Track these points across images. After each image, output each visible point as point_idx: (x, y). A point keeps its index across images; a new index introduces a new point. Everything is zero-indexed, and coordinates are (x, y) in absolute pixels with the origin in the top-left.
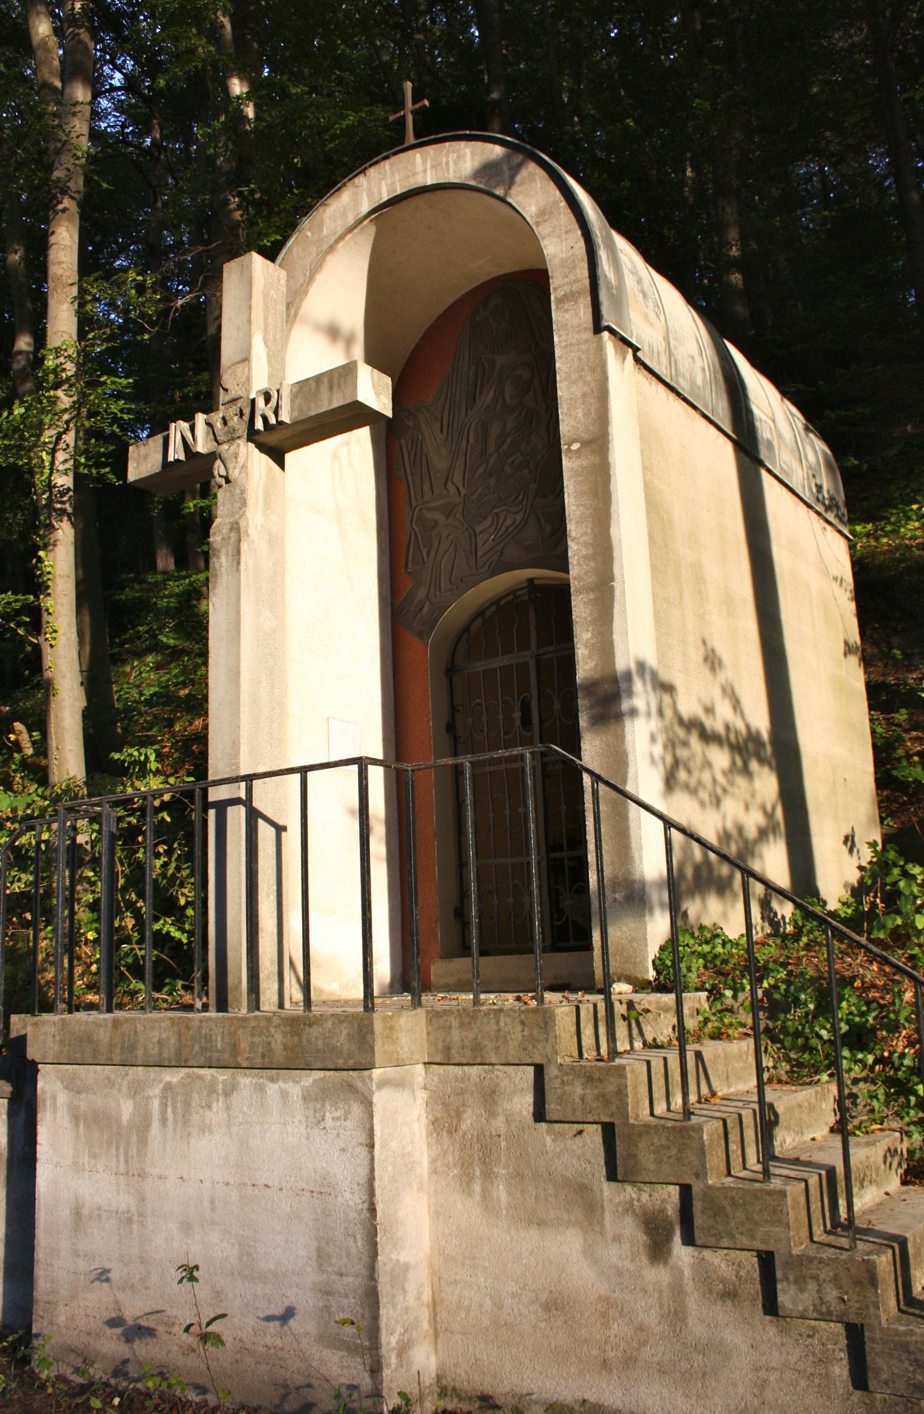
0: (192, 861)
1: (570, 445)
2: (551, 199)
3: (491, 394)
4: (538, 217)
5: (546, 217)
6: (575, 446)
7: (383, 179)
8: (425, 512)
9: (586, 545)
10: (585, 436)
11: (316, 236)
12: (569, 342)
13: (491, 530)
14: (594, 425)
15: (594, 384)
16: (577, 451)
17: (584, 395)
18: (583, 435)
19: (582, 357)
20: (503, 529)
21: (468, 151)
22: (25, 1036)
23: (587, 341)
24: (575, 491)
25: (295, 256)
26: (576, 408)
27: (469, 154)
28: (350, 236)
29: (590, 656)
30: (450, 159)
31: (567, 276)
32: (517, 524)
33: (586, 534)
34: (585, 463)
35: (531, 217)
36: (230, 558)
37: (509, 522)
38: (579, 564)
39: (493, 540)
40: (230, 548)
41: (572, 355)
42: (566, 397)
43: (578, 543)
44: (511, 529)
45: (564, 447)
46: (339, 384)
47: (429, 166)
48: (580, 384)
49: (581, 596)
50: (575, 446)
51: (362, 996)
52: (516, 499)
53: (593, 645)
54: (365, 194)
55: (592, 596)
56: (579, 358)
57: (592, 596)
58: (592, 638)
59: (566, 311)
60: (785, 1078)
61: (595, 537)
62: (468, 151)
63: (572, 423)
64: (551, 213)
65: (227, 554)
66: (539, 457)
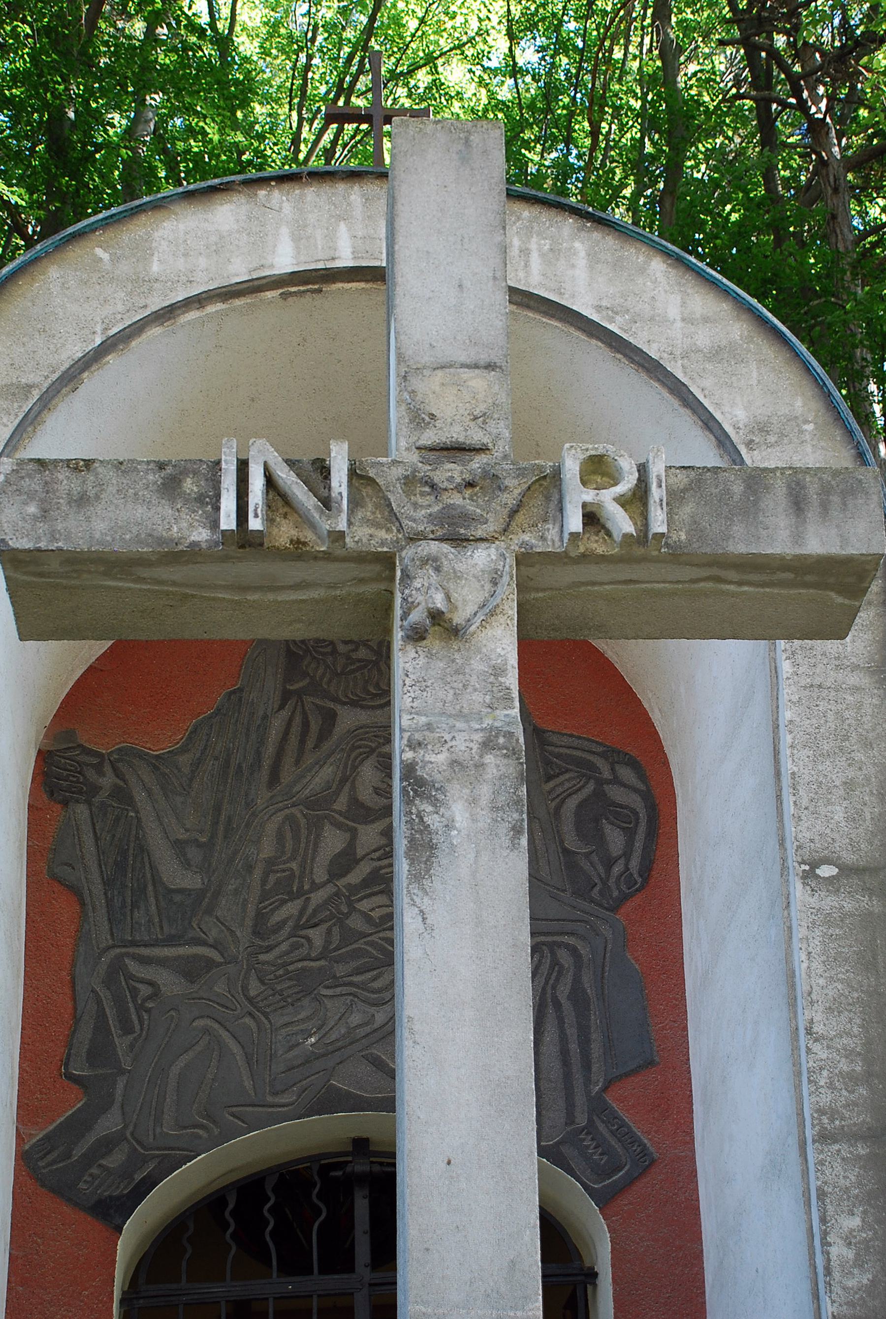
1: (814, 865)
2: (784, 410)
3: (327, 772)
5: (772, 439)
6: (826, 871)
7: (340, 218)
9: (849, 1054)
10: (849, 858)
11: (125, 268)
12: (817, 681)
15: (870, 770)
16: (830, 880)
17: (849, 785)
18: (844, 854)
19: (846, 714)
23: (855, 689)
24: (824, 952)
25: (55, 289)
26: (829, 803)
27: (583, 254)
28: (220, 306)
29: (859, 1263)
33: (848, 1034)
34: (848, 906)
35: (737, 428)
36: (485, 817)
37: (355, 1019)
38: (831, 1086)
40: (485, 791)
41: (823, 706)
42: (807, 778)
43: (828, 1047)
44: (361, 1032)
46: (825, 507)
48: (841, 762)
49: (836, 1147)
50: (826, 871)
52: (374, 979)
54: (285, 231)
55: (862, 1150)
58: (862, 1229)
61: (868, 1043)
63: (819, 827)
64: (782, 435)
65: (473, 801)
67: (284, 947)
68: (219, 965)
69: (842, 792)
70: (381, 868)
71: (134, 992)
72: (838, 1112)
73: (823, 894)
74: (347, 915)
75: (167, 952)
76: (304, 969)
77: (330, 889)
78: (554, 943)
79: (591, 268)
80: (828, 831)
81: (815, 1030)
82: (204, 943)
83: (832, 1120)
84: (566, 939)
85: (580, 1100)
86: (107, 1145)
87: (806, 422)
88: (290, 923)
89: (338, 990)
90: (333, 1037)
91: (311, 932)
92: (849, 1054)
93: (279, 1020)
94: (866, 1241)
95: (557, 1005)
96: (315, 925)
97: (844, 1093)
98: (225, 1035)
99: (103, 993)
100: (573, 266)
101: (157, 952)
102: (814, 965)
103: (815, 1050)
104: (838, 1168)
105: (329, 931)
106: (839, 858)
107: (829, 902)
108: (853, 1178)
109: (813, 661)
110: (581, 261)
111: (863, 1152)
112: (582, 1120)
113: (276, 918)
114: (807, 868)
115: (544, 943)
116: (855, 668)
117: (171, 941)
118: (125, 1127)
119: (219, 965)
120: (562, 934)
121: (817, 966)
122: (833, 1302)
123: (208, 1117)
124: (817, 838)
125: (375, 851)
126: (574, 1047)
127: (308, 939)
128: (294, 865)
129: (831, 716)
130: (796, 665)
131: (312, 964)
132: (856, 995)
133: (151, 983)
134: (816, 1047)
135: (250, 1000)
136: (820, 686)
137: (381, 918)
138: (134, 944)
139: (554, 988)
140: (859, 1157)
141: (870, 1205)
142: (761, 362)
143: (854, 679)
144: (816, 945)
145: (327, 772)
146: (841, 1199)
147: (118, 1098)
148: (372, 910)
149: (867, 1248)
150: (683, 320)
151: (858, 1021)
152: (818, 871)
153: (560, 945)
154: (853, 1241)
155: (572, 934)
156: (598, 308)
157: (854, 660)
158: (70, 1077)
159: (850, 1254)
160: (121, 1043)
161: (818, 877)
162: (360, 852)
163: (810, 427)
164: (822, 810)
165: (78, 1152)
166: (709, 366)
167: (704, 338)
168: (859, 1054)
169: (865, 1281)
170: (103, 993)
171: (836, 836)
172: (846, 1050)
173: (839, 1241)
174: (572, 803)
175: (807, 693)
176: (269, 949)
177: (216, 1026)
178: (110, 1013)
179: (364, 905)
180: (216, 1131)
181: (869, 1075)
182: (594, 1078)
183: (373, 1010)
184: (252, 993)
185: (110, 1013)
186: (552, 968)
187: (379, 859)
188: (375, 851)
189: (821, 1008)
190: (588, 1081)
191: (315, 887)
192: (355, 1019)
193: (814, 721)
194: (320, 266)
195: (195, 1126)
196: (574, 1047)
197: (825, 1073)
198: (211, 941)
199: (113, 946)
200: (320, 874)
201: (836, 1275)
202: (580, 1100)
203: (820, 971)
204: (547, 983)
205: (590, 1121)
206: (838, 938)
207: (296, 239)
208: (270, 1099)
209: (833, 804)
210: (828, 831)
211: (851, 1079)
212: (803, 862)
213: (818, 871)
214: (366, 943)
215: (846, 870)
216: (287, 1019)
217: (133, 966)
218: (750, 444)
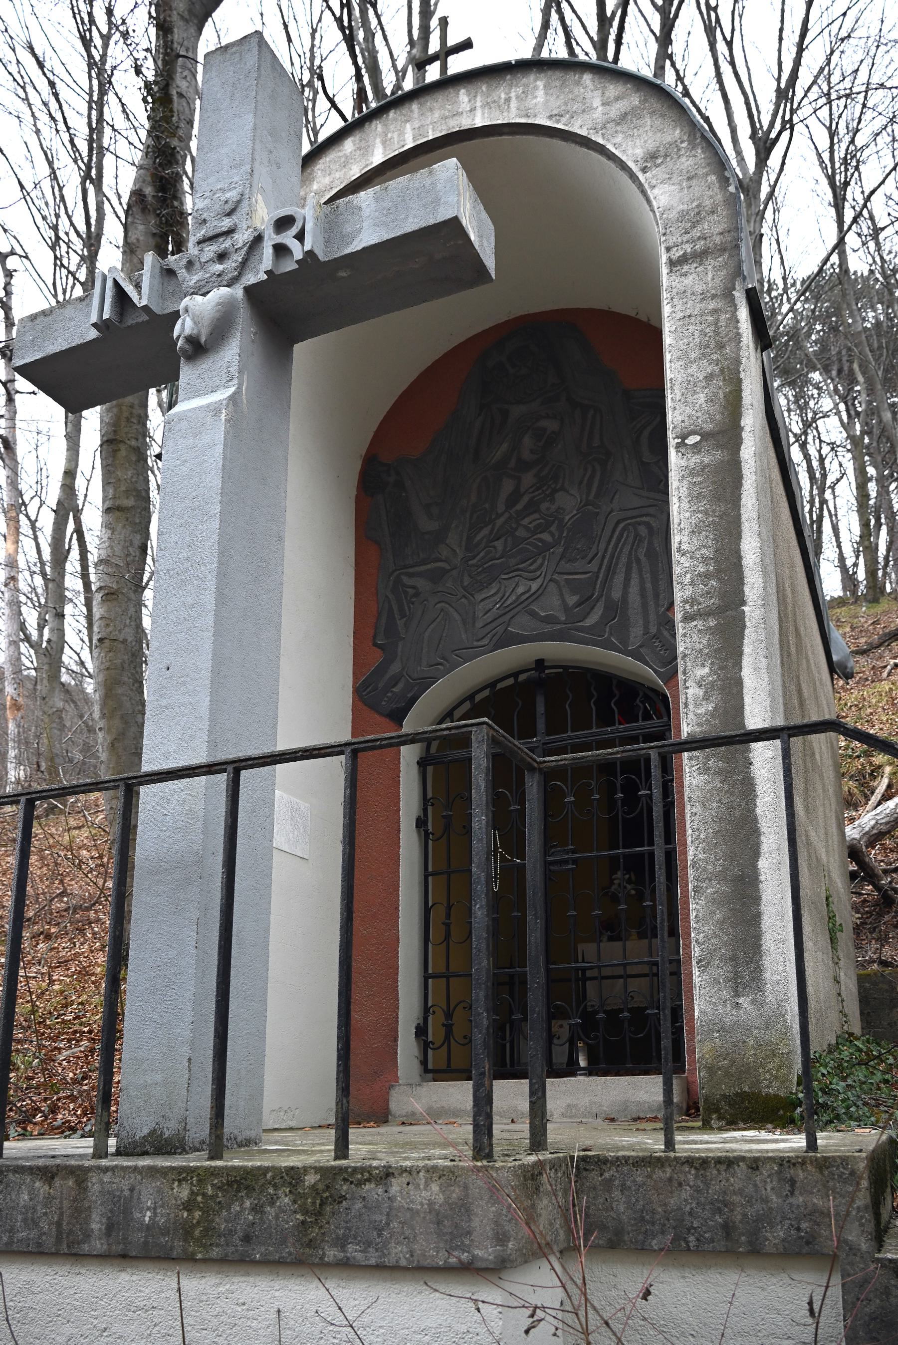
0: (855, 293)
1: (684, 437)
3: (505, 447)
4: (646, 161)
5: (659, 161)
6: (692, 440)
8: (405, 579)
9: (705, 560)
10: (708, 427)
12: (688, 312)
13: (497, 598)
14: (723, 414)
16: (695, 445)
17: (709, 377)
18: (705, 426)
19: (708, 330)
20: (514, 597)
21: (540, 84)
22: (273, 246)
24: (689, 495)
26: (695, 393)
27: (541, 87)
29: (706, 698)
30: (513, 95)
31: (687, 233)
32: (532, 591)
37: (520, 590)
38: (692, 583)
39: (498, 609)
41: (692, 328)
44: (524, 597)
45: (672, 442)
47: (478, 104)
49: (695, 623)
51: (661, 1098)
52: (531, 564)
53: (712, 683)
54: (378, 140)
55: (712, 623)
56: (703, 333)
57: (712, 623)
59: (685, 275)
60: (49, 1242)
62: (540, 84)
63: (688, 411)
64: (666, 156)
66: (567, 518)
67: (482, 554)
68: (449, 571)
69: (704, 384)
70: (534, 497)
71: (406, 593)
72: (696, 600)
73: (689, 456)
74: (516, 529)
75: (422, 568)
76: (492, 565)
77: (507, 515)
78: (636, 523)
79: (546, 94)
80: (694, 412)
81: (683, 547)
82: (441, 561)
83: (692, 606)
84: (644, 519)
85: (652, 617)
86: (395, 680)
87: (682, 142)
88: (485, 540)
89: (511, 575)
90: (508, 602)
91: (496, 543)
92: (705, 560)
93: (479, 597)
94: (712, 682)
95: (638, 561)
96: (498, 539)
97: (701, 586)
98: (451, 609)
99: (391, 596)
100: (536, 97)
101: (417, 569)
102: (683, 505)
103: (682, 561)
104: (695, 637)
105: (506, 540)
106: (701, 428)
107: (694, 460)
108: (705, 642)
109: (685, 300)
110: (540, 93)
111: (712, 624)
112: (653, 630)
113: (478, 538)
114: (680, 440)
115: (629, 524)
116: (714, 297)
117: (424, 562)
118: (403, 669)
119: (449, 571)
120: (641, 516)
121: (685, 505)
122: (688, 724)
123: (443, 658)
124: (686, 419)
125: (531, 487)
126: (648, 585)
127: (495, 547)
128: (487, 506)
129: (697, 334)
130: (674, 306)
131: (497, 561)
132: (711, 519)
133: (414, 587)
134: (683, 559)
135: (464, 588)
136: (690, 316)
137: (535, 527)
138: (406, 567)
139: (636, 551)
140: (710, 628)
141: (716, 658)
142: (652, 113)
143: (712, 305)
144: (684, 491)
145: (505, 447)
146: (697, 658)
147: (399, 653)
148: (530, 523)
149: (713, 687)
150: (603, 104)
151: (712, 537)
152: (686, 441)
153: (639, 523)
154: (704, 683)
155: (647, 515)
156: (550, 117)
157: (713, 291)
158: (375, 645)
159: (701, 692)
160: (400, 623)
161: (686, 445)
162: (522, 490)
163: (684, 145)
164: (690, 399)
165: (381, 685)
166: (619, 128)
167: (615, 110)
168: (712, 559)
169: (710, 708)
170: (391, 596)
171: (699, 414)
172: (703, 557)
173: (694, 684)
174: (646, 433)
175: (681, 323)
176: (474, 557)
177: (447, 606)
178: (395, 607)
179: (525, 522)
180: (448, 665)
181: (718, 571)
182: (661, 603)
183: (530, 583)
184: (466, 584)
185: (395, 607)
186: (635, 538)
187: (533, 492)
188: (531, 487)
189: (687, 533)
190: (657, 605)
191: (499, 516)
192: (520, 590)
193: (685, 340)
194: (397, 153)
195: (438, 664)
196: (648, 585)
197: (688, 576)
198: (443, 558)
199: (396, 570)
200: (501, 508)
201: (691, 707)
202: (652, 617)
203: (686, 509)
204: (632, 548)
205: (659, 630)
206: (700, 483)
207: (384, 143)
208: (476, 643)
209: (697, 393)
210: (694, 412)
211: (706, 576)
212: (677, 437)
213: (686, 441)
214: (527, 544)
215: (705, 436)
216: (483, 596)
217: (405, 579)
218: (644, 170)
